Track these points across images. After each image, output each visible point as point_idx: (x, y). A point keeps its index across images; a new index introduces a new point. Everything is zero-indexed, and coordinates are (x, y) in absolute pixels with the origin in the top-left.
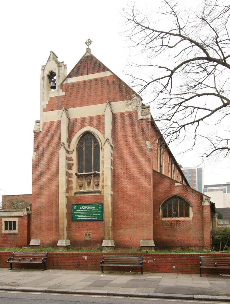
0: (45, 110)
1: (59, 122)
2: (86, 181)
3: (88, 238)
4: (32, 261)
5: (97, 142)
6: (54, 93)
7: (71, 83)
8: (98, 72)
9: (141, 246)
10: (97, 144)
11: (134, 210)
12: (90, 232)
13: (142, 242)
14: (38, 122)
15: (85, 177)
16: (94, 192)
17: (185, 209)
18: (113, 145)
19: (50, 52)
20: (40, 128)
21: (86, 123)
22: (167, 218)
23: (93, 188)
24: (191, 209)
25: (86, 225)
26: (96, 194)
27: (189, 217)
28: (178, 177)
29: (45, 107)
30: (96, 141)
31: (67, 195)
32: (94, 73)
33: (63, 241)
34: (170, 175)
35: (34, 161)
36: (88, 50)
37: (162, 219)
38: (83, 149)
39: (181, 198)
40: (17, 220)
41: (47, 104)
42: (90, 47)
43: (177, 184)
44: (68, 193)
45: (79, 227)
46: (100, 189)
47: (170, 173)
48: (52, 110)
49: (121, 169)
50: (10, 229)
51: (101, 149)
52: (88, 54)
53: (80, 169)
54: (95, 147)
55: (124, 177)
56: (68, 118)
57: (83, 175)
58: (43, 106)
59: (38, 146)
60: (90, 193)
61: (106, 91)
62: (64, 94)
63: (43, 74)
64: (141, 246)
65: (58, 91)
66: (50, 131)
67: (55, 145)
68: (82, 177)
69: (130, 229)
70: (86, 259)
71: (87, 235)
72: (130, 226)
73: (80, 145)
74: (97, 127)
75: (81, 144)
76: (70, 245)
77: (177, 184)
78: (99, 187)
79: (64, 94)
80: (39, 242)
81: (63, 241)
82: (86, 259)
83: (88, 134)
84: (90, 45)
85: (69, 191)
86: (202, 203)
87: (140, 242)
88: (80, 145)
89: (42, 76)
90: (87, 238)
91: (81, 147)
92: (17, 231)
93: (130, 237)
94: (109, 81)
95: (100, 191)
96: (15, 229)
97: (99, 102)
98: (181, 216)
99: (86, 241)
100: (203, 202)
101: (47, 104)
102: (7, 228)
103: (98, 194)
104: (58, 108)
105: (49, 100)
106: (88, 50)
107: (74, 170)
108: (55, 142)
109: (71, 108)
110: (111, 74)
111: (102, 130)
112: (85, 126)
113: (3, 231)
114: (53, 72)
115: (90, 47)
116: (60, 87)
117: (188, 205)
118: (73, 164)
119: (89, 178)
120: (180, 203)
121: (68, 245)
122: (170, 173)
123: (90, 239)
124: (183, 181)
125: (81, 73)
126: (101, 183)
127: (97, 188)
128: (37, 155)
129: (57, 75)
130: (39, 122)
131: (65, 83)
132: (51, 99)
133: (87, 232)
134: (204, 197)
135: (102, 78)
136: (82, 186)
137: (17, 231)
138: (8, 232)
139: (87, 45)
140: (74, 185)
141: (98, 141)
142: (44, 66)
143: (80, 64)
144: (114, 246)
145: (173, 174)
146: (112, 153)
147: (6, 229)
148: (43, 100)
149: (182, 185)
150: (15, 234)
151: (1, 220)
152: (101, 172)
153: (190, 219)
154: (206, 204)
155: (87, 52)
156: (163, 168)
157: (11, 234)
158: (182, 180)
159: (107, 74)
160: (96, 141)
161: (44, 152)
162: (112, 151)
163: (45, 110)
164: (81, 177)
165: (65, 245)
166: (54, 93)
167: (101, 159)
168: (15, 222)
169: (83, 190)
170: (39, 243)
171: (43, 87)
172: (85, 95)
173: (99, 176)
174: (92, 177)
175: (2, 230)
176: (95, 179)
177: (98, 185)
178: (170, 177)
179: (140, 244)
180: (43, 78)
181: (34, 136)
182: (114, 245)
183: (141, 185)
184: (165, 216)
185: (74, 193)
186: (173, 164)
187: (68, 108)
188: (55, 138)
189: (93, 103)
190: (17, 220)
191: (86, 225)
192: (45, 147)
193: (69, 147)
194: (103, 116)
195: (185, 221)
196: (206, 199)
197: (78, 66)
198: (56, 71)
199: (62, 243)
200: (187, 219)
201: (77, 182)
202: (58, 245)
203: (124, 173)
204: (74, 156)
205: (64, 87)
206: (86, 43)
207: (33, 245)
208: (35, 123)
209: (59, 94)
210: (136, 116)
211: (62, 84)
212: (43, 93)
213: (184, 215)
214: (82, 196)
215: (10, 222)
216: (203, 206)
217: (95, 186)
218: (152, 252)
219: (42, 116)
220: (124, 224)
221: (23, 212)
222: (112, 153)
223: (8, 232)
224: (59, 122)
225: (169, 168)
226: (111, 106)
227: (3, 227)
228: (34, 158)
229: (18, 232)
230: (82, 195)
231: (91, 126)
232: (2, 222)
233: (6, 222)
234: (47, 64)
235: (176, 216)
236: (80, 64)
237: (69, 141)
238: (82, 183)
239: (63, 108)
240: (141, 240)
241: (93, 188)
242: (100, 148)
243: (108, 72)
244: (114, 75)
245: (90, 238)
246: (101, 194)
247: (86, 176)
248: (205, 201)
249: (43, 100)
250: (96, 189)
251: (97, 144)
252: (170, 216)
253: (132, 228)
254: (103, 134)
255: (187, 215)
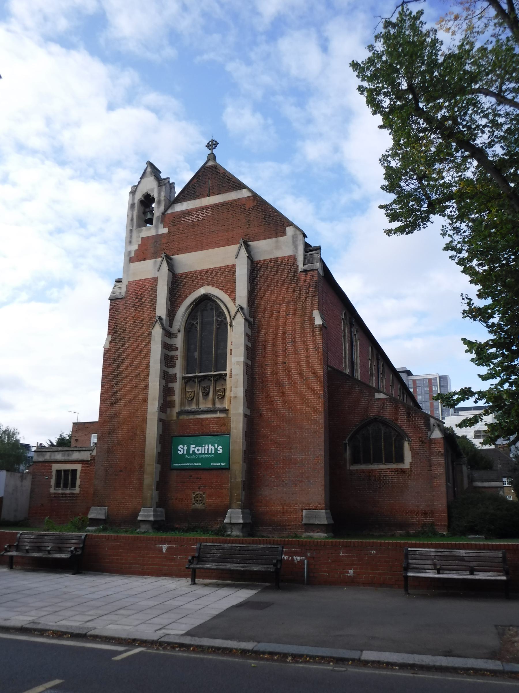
0: (131, 260)
1: (155, 280)
2: (200, 390)
3: (199, 506)
4: (51, 552)
5: (223, 315)
6: (149, 231)
7: (180, 211)
8: (226, 191)
9: (305, 524)
10: (222, 318)
11: (291, 448)
12: (204, 494)
13: (306, 514)
14: (119, 281)
15: (199, 382)
16: (214, 411)
17: (395, 447)
18: (252, 320)
19: (146, 164)
20: (123, 290)
21: (203, 280)
22: (361, 464)
23: (214, 403)
24: (406, 445)
25: (197, 478)
26: (218, 415)
27: (404, 463)
28: (392, 386)
29: (133, 255)
30: (221, 313)
31: (163, 416)
32: (220, 194)
33: (148, 511)
34: (374, 381)
35: (107, 352)
36: (212, 157)
37: (350, 466)
38: (196, 327)
39: (386, 423)
40: (78, 467)
41: (137, 248)
42: (215, 151)
43: (378, 396)
44: (166, 413)
45: (184, 483)
46: (226, 405)
47: (374, 378)
48: (144, 259)
49: (266, 365)
50: (66, 486)
51: (229, 327)
52: (211, 163)
53: (189, 367)
54: (218, 325)
55: (271, 381)
56: (171, 272)
57: (195, 377)
58: (130, 252)
59: (116, 325)
60: (207, 414)
61: (240, 222)
62: (165, 231)
63: (133, 199)
64: (303, 522)
65: (157, 227)
66: (139, 297)
67: (146, 322)
68: (193, 381)
69: (283, 486)
70: (164, 550)
71: (199, 499)
72: (283, 481)
73: (192, 322)
74: (224, 286)
75: (193, 319)
76: (164, 519)
77: (378, 396)
78: (225, 402)
79: (165, 231)
80: (107, 511)
81: (148, 511)
82: (164, 550)
83: (206, 298)
84: (215, 148)
85: (168, 410)
86: (429, 433)
87: (302, 516)
88: (192, 322)
89: (131, 202)
90: (198, 505)
91: (193, 324)
92: (77, 490)
93: (281, 504)
94: (246, 206)
95: (225, 408)
96: (73, 485)
97: (228, 242)
98: (388, 460)
99: (196, 511)
100: (430, 430)
101: (137, 248)
102: (60, 484)
103: (223, 415)
104: (154, 256)
105: (140, 243)
106: (212, 157)
107: (178, 370)
108: (146, 316)
109: (178, 254)
110: (249, 194)
111: (231, 292)
112: (201, 286)
113: (52, 490)
114: (150, 195)
115: (215, 151)
116: (160, 220)
117: (400, 437)
118: (176, 357)
119: (205, 383)
120: (385, 433)
121: (159, 519)
122: (374, 378)
123: (203, 507)
124: (405, 396)
125: (197, 194)
126: (227, 393)
127: (222, 404)
128: (112, 342)
129: (156, 199)
130: (121, 282)
131: (169, 211)
132: (143, 239)
133: (198, 492)
134: (432, 421)
135: (235, 201)
136: (193, 398)
137: (77, 490)
138: (60, 491)
139: (210, 150)
140: (177, 398)
141: (225, 314)
142: (135, 186)
143: (196, 181)
144: (250, 523)
145: (380, 380)
146: (250, 334)
147: (58, 485)
148: (130, 242)
149: (387, 397)
150: (72, 495)
151: (51, 467)
152: (228, 372)
153: (406, 467)
154: (437, 434)
155: (208, 160)
156: (358, 368)
157: (65, 494)
158: (403, 394)
159: (245, 194)
160: (220, 312)
161: (126, 336)
162: (249, 332)
163: (131, 260)
164: (191, 381)
165: (152, 519)
166: (149, 231)
167: (229, 347)
168: (74, 472)
169: (194, 407)
170: (107, 515)
171: (132, 220)
172: (203, 231)
173: (225, 380)
174: (211, 381)
175: (51, 486)
176: (217, 385)
177: (223, 397)
178: (374, 386)
179: (302, 520)
180: (132, 206)
181: (110, 306)
182: (249, 521)
183: (304, 396)
184: (355, 460)
185: (177, 413)
186: (379, 361)
187: (173, 255)
188: (147, 310)
189: (218, 245)
190: (78, 467)
191: (197, 478)
192: (128, 325)
193: (171, 325)
194: (234, 266)
195: (397, 470)
196: (436, 425)
197: (193, 182)
198: (155, 195)
199: (149, 516)
200: (401, 466)
201: (184, 391)
202: (139, 518)
203: (272, 373)
204: (179, 341)
205: (167, 220)
206: (208, 146)
207: (94, 518)
208: (113, 283)
209: (157, 231)
210: (295, 266)
211: (163, 214)
212: (131, 231)
213: (394, 459)
214: (191, 419)
215: (66, 471)
216: (431, 440)
217: (217, 400)
218: (320, 536)
219: (126, 270)
220: (271, 477)
221: (91, 452)
222: (250, 334)
223: (60, 491)
224: (155, 280)
225: (371, 369)
226: (249, 248)
227: (53, 482)
228: (108, 346)
229: (79, 492)
230: (191, 417)
231: (212, 285)
232: (51, 472)
233: (58, 472)
234: (139, 182)
235: (378, 461)
236: (196, 181)
237: (171, 313)
238: (193, 393)
239: (163, 255)
240: (304, 511)
241: (214, 403)
242: (229, 325)
243: (245, 190)
244: (255, 197)
245: (203, 504)
246: (227, 414)
247: (201, 380)
248: (434, 430)
249: (130, 242)
250: (218, 405)
251: (222, 318)
252: (368, 461)
253: (286, 484)
254: (233, 299)
255: (400, 459)
